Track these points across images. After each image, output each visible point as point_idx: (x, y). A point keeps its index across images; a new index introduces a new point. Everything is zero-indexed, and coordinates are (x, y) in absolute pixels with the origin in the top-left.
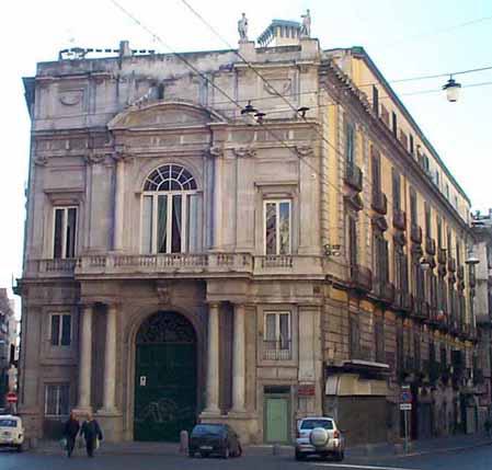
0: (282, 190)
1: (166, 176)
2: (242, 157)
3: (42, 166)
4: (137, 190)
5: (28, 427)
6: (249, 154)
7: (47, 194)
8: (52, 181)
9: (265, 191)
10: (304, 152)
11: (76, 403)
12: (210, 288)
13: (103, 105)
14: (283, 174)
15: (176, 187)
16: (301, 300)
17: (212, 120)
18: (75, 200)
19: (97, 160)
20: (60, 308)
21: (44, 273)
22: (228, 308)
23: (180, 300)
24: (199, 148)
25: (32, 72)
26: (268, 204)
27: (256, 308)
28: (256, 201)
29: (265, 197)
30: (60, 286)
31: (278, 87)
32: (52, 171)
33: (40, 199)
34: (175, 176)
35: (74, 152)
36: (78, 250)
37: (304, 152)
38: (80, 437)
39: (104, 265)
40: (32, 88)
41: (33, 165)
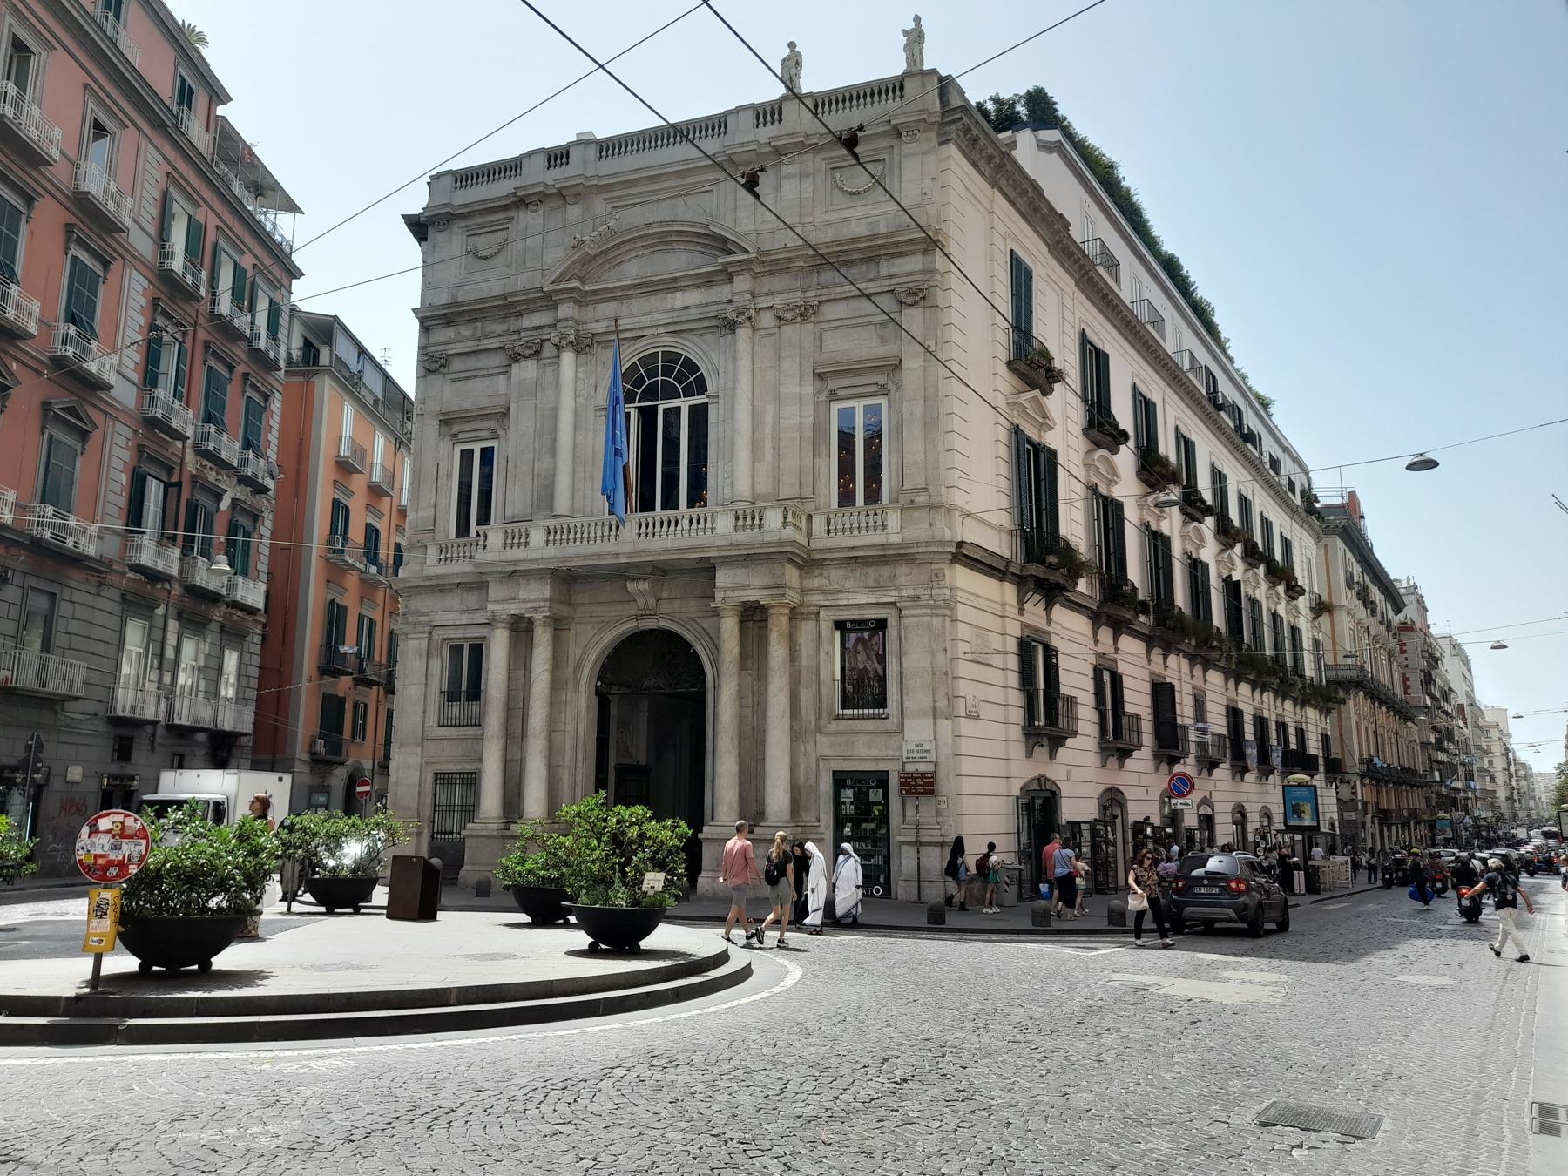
0: (480, 425)
1: (652, 373)
2: (789, 322)
6: (805, 313)
7: (819, 376)
9: (833, 384)
11: (1531, 874)
12: (723, 578)
13: (540, 249)
15: (672, 393)
17: (730, 253)
18: (494, 431)
19: (910, 300)
22: (753, 616)
23: (672, 613)
24: (712, 311)
25: (418, 201)
28: (817, 405)
29: (834, 396)
31: (484, 243)
32: (453, 380)
34: (667, 371)
39: (884, 527)
41: (423, 372)
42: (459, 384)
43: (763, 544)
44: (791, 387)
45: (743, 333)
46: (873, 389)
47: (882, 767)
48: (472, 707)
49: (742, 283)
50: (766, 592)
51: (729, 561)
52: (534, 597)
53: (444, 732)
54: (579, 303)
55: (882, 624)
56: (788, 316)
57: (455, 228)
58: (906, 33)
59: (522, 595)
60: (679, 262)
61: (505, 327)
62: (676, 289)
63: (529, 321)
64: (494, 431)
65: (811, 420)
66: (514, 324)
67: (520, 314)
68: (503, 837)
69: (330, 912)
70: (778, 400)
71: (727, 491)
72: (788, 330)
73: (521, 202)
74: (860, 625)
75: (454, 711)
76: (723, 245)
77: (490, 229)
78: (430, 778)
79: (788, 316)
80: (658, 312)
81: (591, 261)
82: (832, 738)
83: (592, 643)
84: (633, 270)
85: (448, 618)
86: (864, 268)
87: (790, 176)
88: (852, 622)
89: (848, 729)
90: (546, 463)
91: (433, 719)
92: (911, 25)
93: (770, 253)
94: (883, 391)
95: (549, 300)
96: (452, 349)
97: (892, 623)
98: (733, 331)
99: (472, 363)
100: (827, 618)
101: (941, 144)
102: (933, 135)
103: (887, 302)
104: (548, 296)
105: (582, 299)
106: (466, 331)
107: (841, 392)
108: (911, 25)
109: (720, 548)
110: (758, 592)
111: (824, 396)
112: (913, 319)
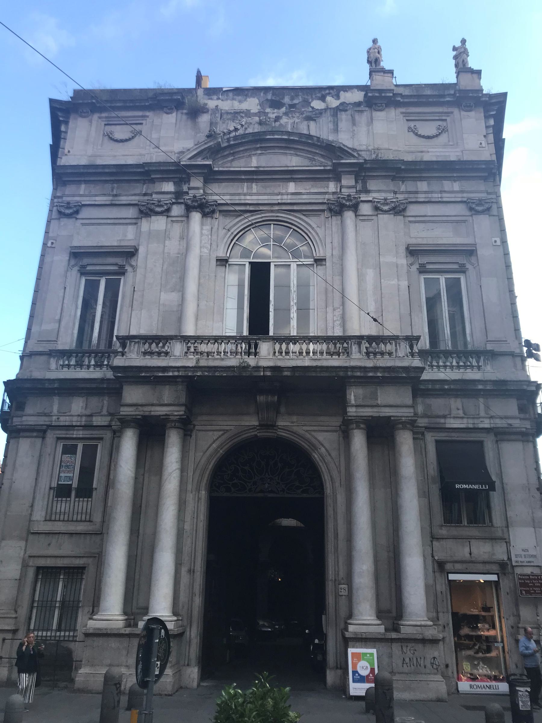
2: (386, 212)
3: (69, 216)
4: (221, 254)
5: (531, 438)
6: (398, 210)
7: (412, 252)
8: (86, 237)
9: (423, 260)
10: (480, 208)
12: (353, 395)
14: (444, 236)
16: (500, 423)
18: (463, 265)
20: (80, 434)
21: (55, 371)
25: (65, 96)
26: (424, 278)
27: (423, 434)
30: (94, 389)
33: (61, 259)
35: (124, 199)
36: (119, 330)
37: (480, 208)
38: (339, 666)
40: (61, 113)
41: (55, 215)
44: (388, 259)
45: (349, 215)
46: (456, 266)
48: (83, 504)
49: (348, 181)
52: (166, 403)
58: (455, 49)
60: (293, 161)
64: (122, 267)
65: (406, 283)
72: (384, 218)
75: (62, 506)
76: (332, 150)
78: (31, 573)
83: (216, 434)
90: (169, 298)
91: (39, 514)
92: (458, 44)
108: (458, 44)
112: (483, 223)
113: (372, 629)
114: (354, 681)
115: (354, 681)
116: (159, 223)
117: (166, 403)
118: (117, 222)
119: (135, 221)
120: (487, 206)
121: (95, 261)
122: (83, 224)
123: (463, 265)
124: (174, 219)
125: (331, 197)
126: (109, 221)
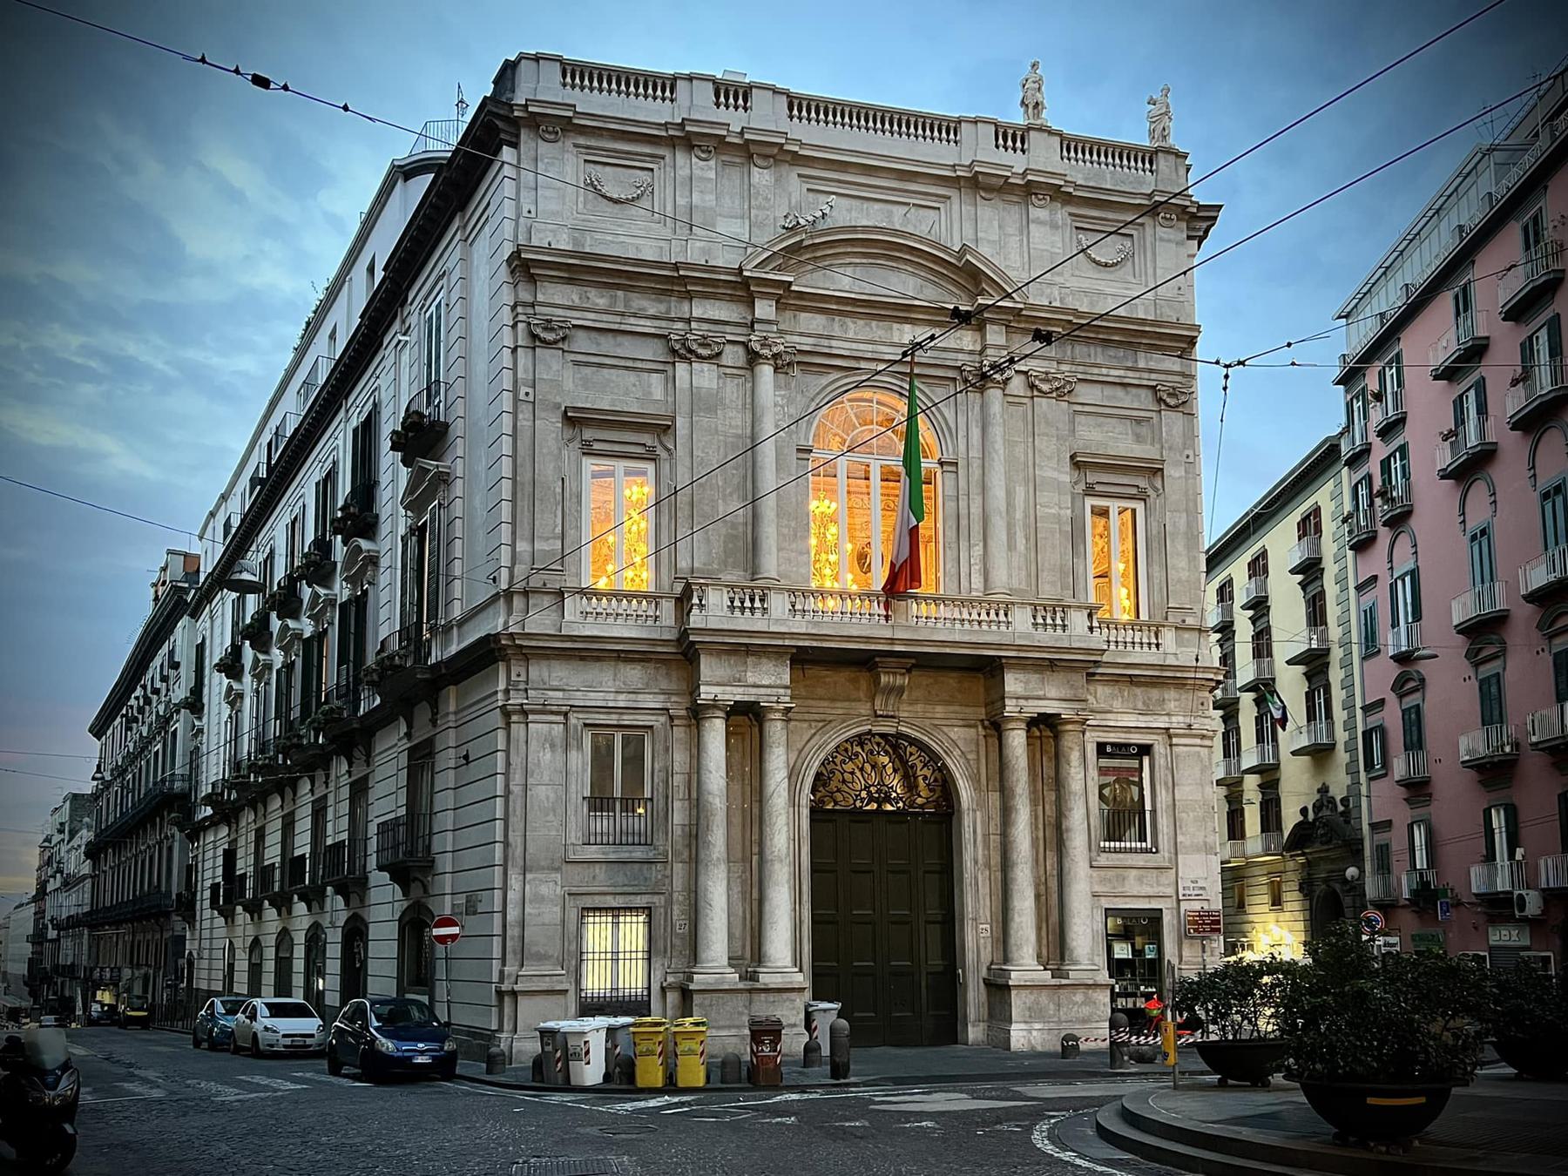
7: (1077, 464)
14: (1121, 443)
18: (652, 450)
29: (1090, 491)
31: (615, 182)
42: (588, 371)
43: (1069, 650)
45: (994, 394)
46: (1134, 491)
47: (1154, 905)
50: (1064, 705)
51: (1022, 664)
53: (592, 852)
54: (781, 306)
55: (1146, 750)
56: (1045, 387)
57: (569, 143)
59: (751, 678)
60: (903, 285)
61: (662, 308)
62: (907, 320)
63: (700, 309)
66: (684, 309)
67: (690, 296)
68: (750, 991)
69: (1222, 1085)
70: (1035, 485)
71: (977, 581)
73: (686, 139)
74: (1121, 750)
75: (602, 824)
76: (971, 276)
77: (622, 162)
79: (1045, 387)
80: (884, 344)
81: (803, 248)
82: (1102, 873)
84: (843, 281)
85: (595, 699)
86: (1121, 353)
87: (1039, 222)
88: (1113, 745)
89: (1117, 863)
91: (575, 836)
93: (1033, 307)
94: (1143, 498)
95: (742, 289)
96: (577, 318)
97: (1160, 749)
98: (982, 390)
99: (607, 345)
100: (1092, 738)
101: (1189, 238)
102: (1184, 225)
103: (1146, 398)
104: (746, 283)
105: (786, 298)
106: (599, 299)
107: (596, 446)
109: (1020, 647)
110: (1056, 704)
111: (1081, 487)
112: (1172, 422)
113: (1034, 975)
114: (611, 1031)
115: (611, 1031)
116: (705, 376)
117: (767, 682)
118: (631, 366)
119: (665, 368)
120: (1183, 398)
121: (1105, 478)
122: (577, 363)
123: (652, 450)
124: (728, 371)
125: (967, 357)
126: (623, 363)
